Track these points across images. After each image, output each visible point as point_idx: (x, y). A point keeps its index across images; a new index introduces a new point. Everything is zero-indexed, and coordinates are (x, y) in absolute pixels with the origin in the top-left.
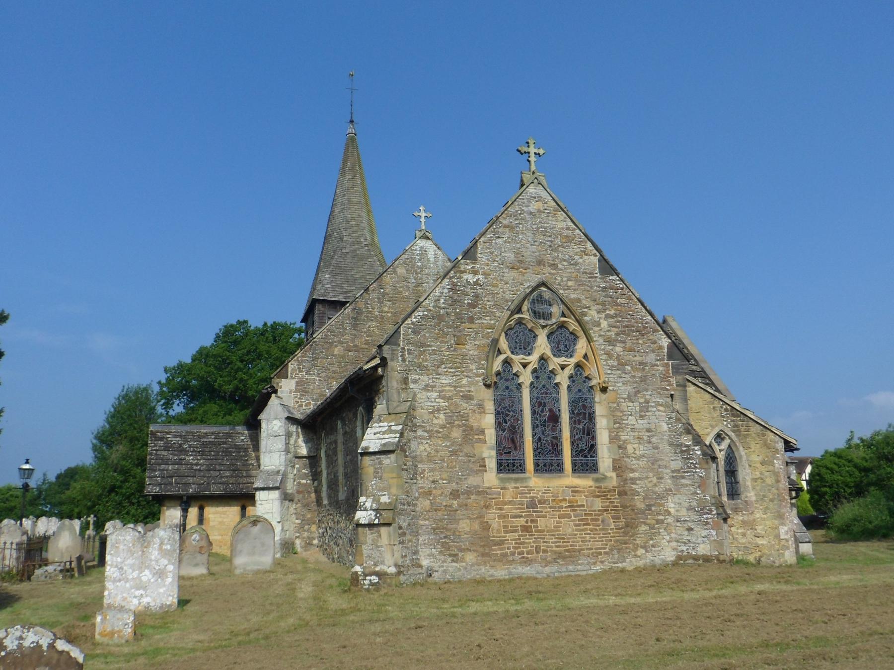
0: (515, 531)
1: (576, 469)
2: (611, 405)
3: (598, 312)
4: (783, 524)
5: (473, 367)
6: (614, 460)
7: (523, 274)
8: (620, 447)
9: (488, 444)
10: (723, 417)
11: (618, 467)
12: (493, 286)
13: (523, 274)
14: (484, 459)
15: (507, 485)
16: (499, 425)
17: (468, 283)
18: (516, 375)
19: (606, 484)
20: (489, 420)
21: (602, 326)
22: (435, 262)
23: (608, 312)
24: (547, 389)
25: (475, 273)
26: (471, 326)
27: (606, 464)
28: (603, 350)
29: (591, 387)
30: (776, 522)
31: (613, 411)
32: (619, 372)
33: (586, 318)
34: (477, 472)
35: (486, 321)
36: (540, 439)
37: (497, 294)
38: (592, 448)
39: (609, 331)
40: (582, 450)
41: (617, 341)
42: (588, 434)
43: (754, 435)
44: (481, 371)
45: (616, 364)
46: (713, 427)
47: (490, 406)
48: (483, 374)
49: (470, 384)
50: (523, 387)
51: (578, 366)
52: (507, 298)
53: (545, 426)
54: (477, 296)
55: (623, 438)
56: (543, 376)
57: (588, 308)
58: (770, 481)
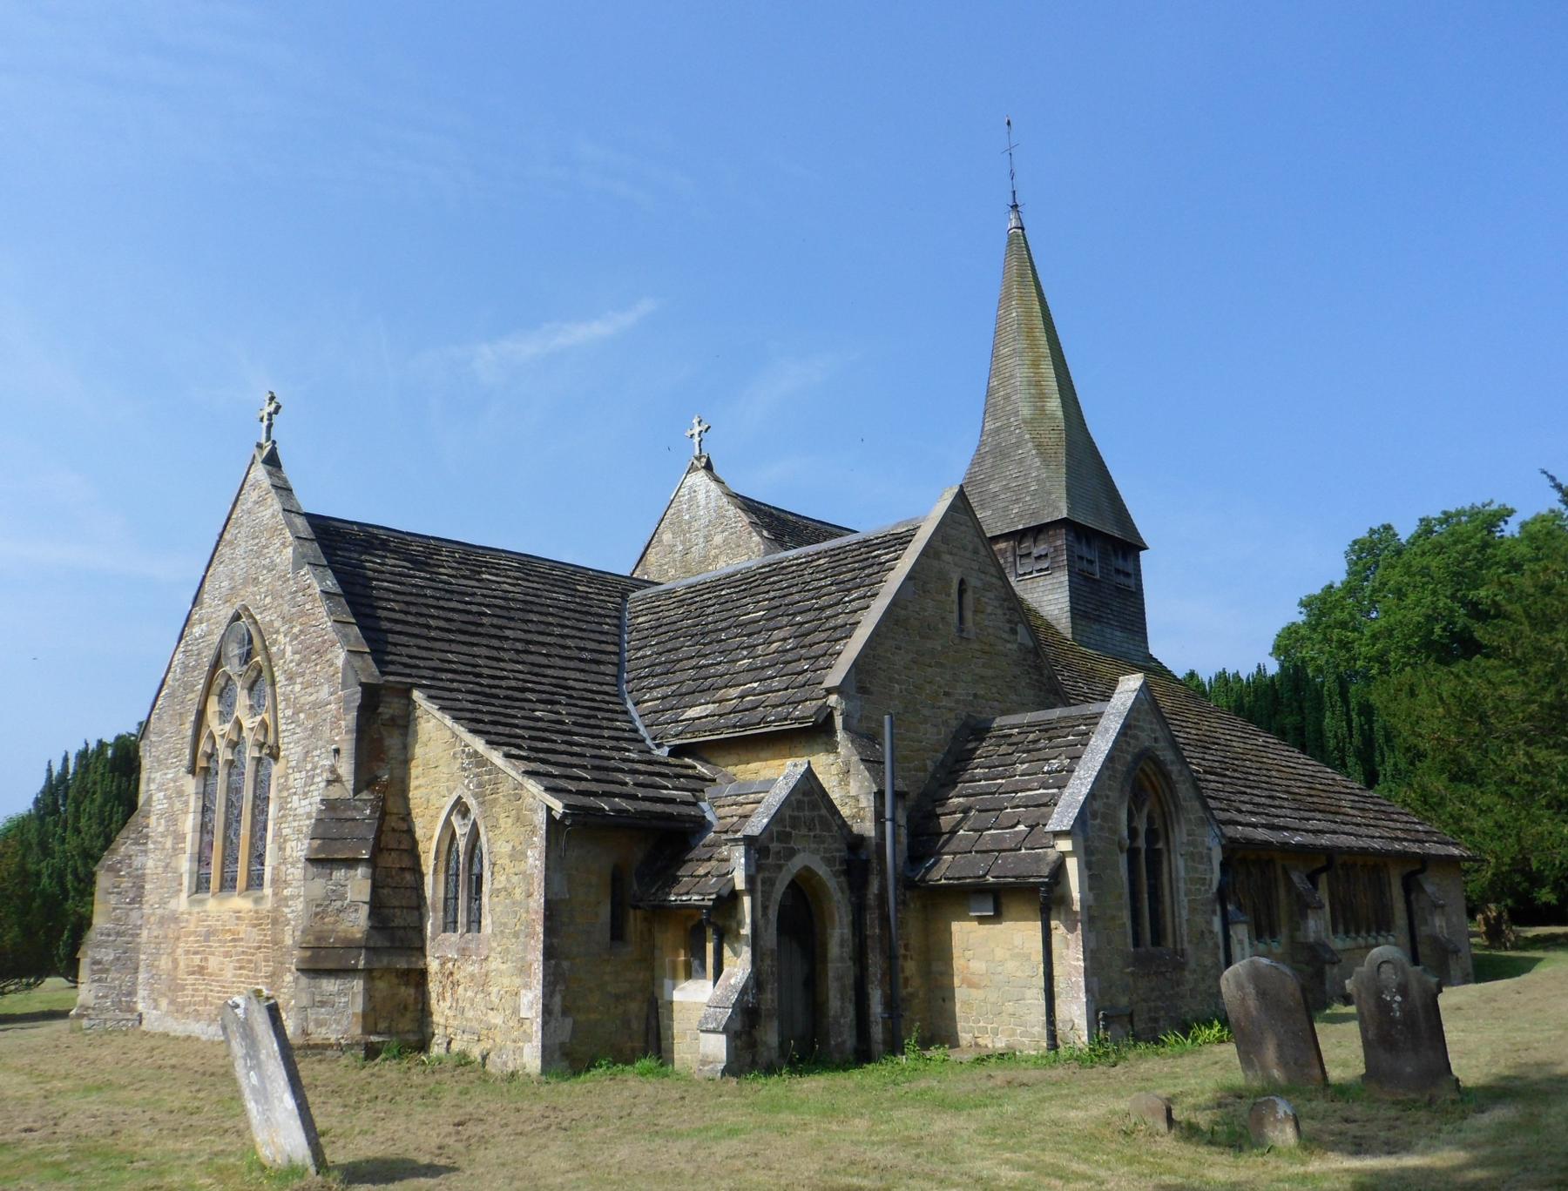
0: (193, 973)
4: (527, 986)
10: (464, 769)
20: (189, 823)
22: (706, 507)
30: (518, 981)
33: (274, 649)
43: (503, 800)
46: (450, 791)
47: (194, 803)
58: (518, 894)
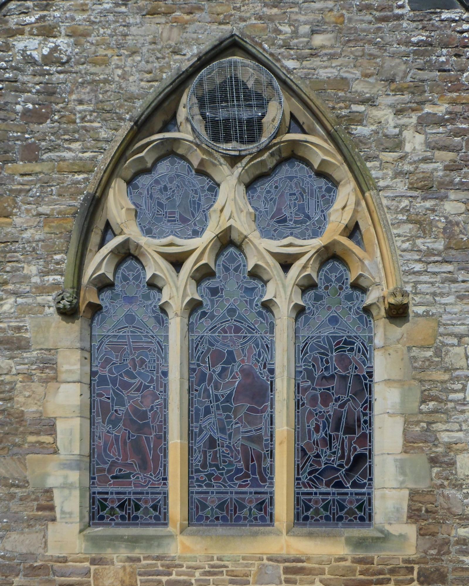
1: (305, 514)
2: (415, 352)
3: (399, 112)
5: (31, 269)
6: (413, 494)
7: (183, 26)
8: (434, 461)
9: (63, 455)
11: (422, 510)
12: (95, 63)
13: (183, 26)
14: (49, 491)
15: (108, 553)
16: (98, 410)
17: (30, 61)
18: (154, 285)
19: (384, 554)
20: (66, 401)
21: (408, 148)
23: (428, 109)
24: (241, 319)
25: (47, 32)
26: (29, 167)
27: (390, 504)
28: (405, 210)
29: (367, 310)
31: (423, 369)
32: (450, 268)
33: (359, 130)
34: (30, 523)
35: (73, 152)
36: (212, 443)
37: (106, 81)
38: (360, 463)
39: (425, 160)
40: (330, 469)
41: (450, 185)
42: (350, 430)
44: (51, 279)
45: (440, 245)
47: (72, 365)
48: (56, 285)
49: (23, 311)
50: (171, 314)
51: (330, 256)
52: (134, 89)
53: (226, 409)
54: (50, 92)
55: (445, 437)
56: (232, 286)
57: (370, 102)
